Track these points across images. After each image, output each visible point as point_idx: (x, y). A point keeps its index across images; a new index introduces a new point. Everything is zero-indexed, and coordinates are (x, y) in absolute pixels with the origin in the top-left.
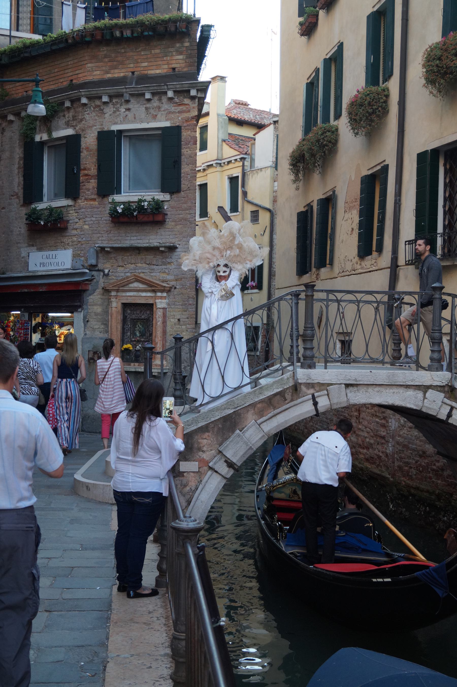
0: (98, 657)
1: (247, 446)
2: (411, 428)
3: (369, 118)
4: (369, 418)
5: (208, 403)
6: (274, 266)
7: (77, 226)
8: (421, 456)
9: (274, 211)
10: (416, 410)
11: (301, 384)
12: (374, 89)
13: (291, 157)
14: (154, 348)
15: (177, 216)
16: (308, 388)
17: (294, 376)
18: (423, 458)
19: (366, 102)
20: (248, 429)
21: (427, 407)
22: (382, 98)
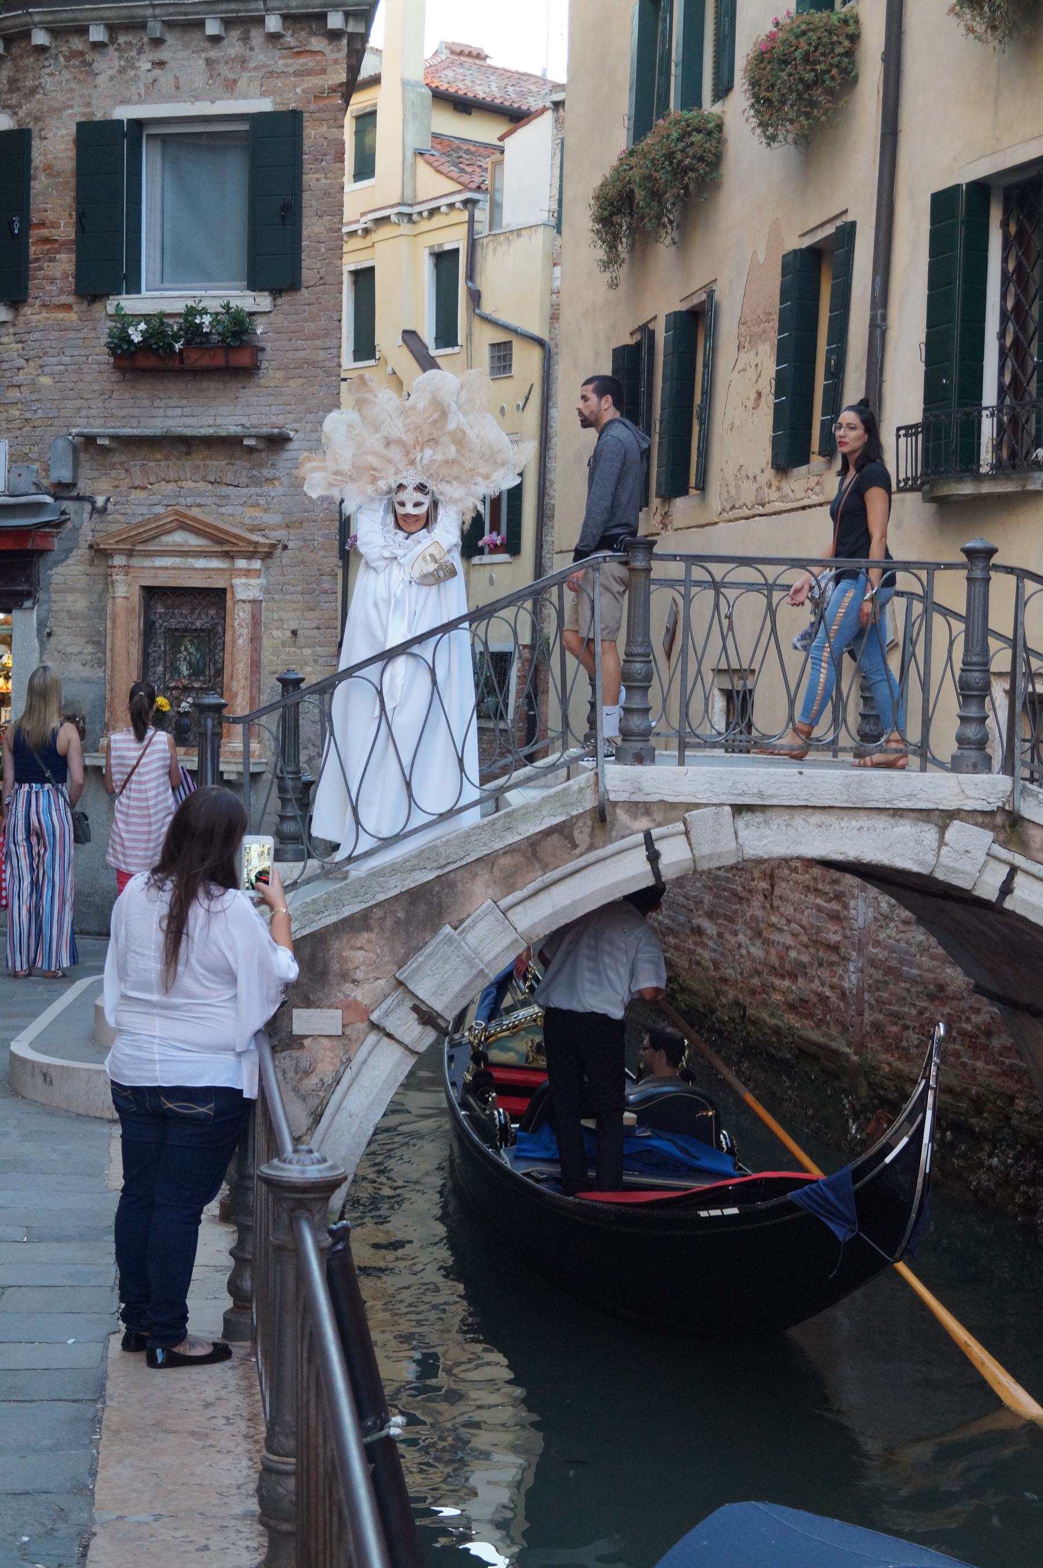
0: (66, 1521)
1: (471, 967)
2: (906, 922)
3: (806, 96)
4: (796, 896)
5: (368, 854)
6: (552, 492)
7: (21, 377)
8: (932, 998)
9: (552, 344)
10: (918, 875)
11: (615, 804)
12: (819, 17)
13: (597, 198)
14: (224, 706)
15: (289, 354)
16: (635, 817)
17: (597, 784)
18: (937, 1002)
19: (797, 54)
21: (947, 867)
22: (840, 43)
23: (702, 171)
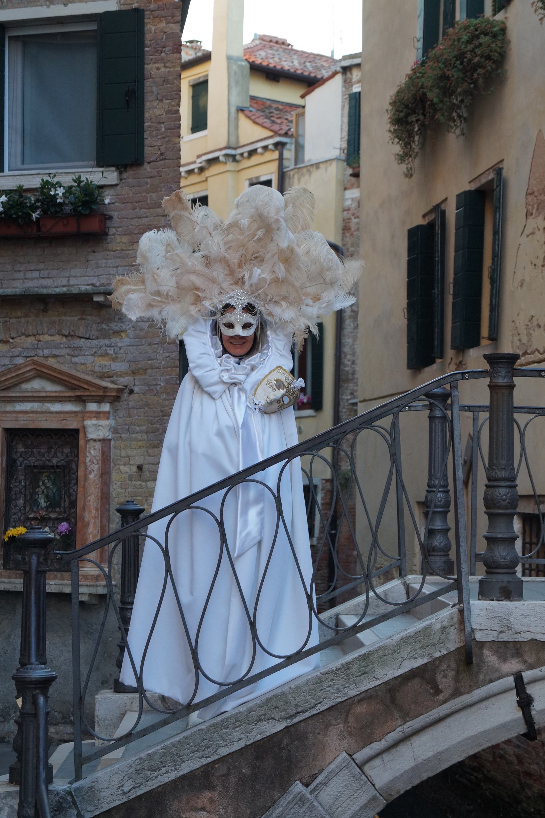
11: (482, 644)
13: (393, 104)
16: (504, 659)
20: (328, 779)
23: (489, 68)
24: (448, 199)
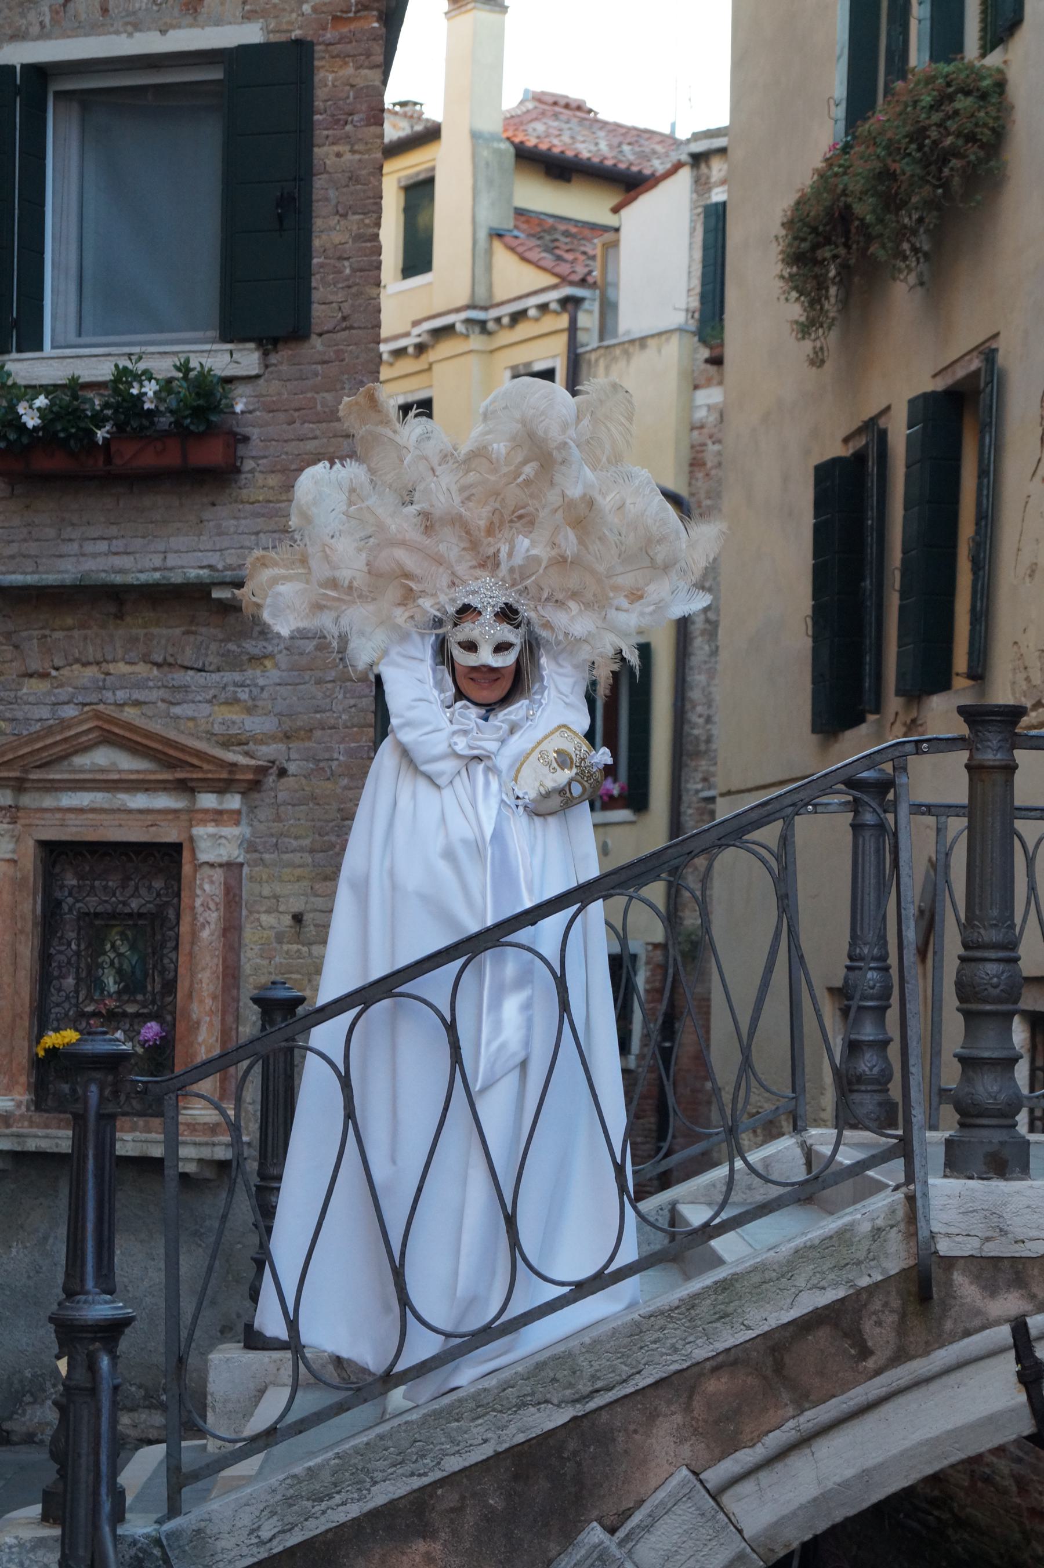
11: (950, 1262)
13: (788, 225)
15: (290, 447)
16: (992, 1290)
20: (653, 1520)
23: (972, 157)
24: (893, 407)
